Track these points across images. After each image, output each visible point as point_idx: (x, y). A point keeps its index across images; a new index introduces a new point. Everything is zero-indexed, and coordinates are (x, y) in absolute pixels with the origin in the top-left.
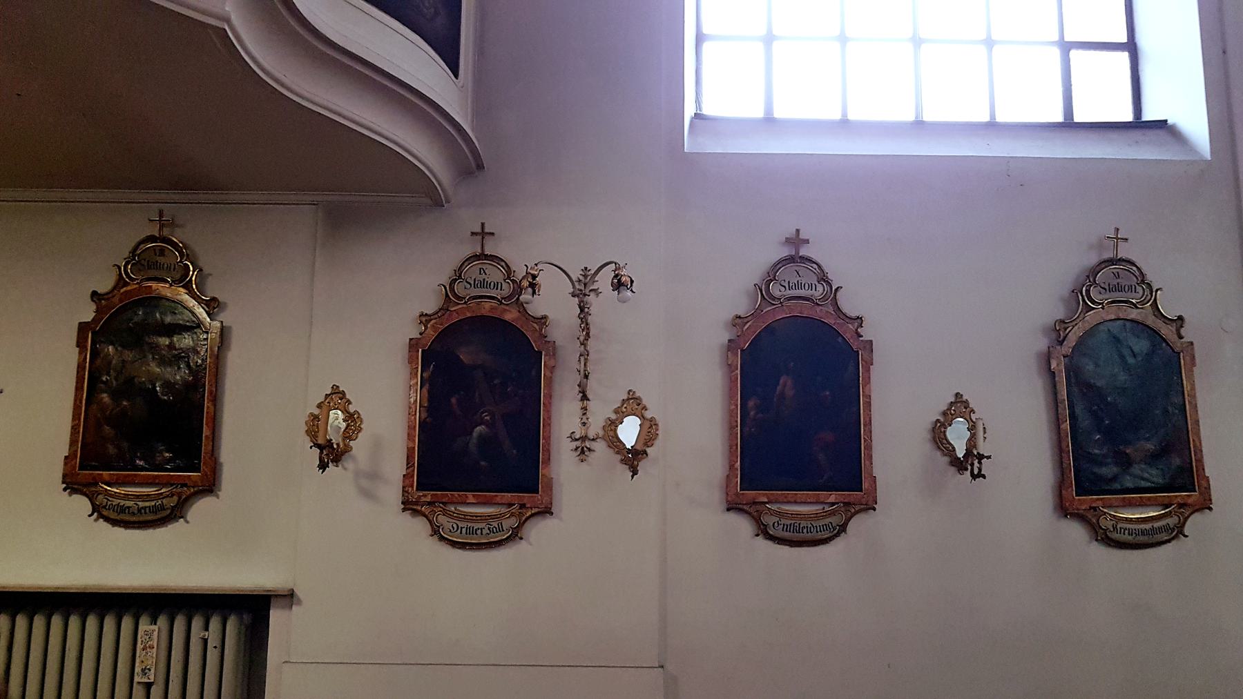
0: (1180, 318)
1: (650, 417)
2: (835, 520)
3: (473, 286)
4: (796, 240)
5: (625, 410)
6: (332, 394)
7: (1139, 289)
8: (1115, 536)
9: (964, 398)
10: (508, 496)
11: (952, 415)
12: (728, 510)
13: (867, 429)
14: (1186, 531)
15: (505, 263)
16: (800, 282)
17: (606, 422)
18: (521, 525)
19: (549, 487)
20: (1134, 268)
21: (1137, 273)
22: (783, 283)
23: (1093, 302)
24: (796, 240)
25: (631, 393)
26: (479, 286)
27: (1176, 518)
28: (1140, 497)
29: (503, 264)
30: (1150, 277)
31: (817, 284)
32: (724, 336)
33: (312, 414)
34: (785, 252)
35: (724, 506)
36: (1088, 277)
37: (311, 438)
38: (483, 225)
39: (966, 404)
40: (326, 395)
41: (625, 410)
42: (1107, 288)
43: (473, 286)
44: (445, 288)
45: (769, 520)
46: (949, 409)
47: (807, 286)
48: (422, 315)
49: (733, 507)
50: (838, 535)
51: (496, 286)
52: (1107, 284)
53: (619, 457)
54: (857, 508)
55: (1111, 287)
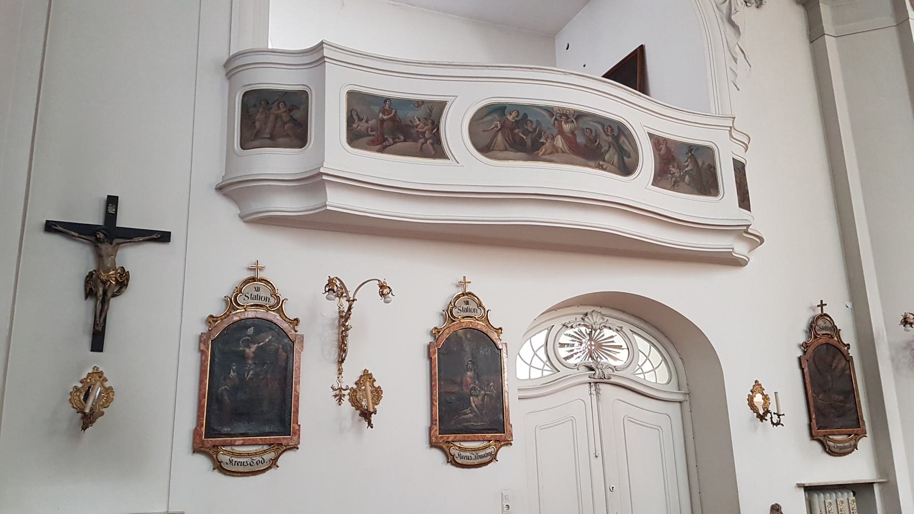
0: (297, 320)
1: (109, 386)
2: (267, 457)
3: (250, 298)
4: (255, 268)
5: (89, 381)
6: (93, 373)
7: (479, 311)
8: (459, 461)
9: (369, 372)
10: (488, 435)
11: (361, 384)
12: (194, 452)
13: (203, 391)
14: (278, 463)
15: (477, 298)
16: (259, 295)
17: (73, 389)
18: (276, 459)
19: (297, 432)
20: (476, 298)
21: (477, 301)
22: (247, 295)
23: (455, 318)
24: (255, 268)
25: (95, 369)
26: (254, 298)
27: (273, 453)
28: (260, 439)
29: (270, 285)
30: (484, 304)
31: (270, 297)
32: (203, 328)
33: (75, 387)
34: (250, 274)
35: (191, 451)
36: (451, 303)
37: (352, 404)
38: (826, 305)
39: (100, 375)
40: (89, 373)
41: (89, 381)
42: (461, 309)
43: (250, 298)
44: (231, 300)
45: (224, 458)
46: (359, 380)
47: (263, 299)
48: (211, 316)
49: (432, 445)
50: (269, 468)
51: (266, 299)
52: (250, 294)
53: (359, 412)
54: (502, 443)
55: (252, 296)
